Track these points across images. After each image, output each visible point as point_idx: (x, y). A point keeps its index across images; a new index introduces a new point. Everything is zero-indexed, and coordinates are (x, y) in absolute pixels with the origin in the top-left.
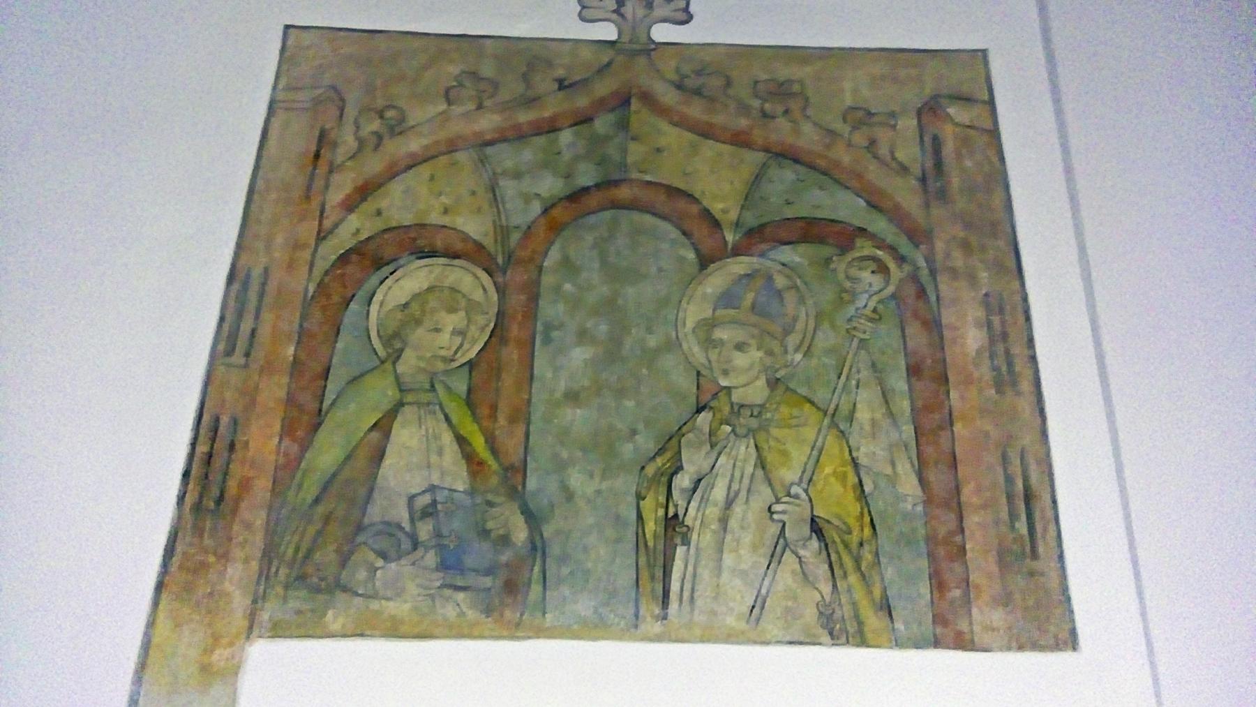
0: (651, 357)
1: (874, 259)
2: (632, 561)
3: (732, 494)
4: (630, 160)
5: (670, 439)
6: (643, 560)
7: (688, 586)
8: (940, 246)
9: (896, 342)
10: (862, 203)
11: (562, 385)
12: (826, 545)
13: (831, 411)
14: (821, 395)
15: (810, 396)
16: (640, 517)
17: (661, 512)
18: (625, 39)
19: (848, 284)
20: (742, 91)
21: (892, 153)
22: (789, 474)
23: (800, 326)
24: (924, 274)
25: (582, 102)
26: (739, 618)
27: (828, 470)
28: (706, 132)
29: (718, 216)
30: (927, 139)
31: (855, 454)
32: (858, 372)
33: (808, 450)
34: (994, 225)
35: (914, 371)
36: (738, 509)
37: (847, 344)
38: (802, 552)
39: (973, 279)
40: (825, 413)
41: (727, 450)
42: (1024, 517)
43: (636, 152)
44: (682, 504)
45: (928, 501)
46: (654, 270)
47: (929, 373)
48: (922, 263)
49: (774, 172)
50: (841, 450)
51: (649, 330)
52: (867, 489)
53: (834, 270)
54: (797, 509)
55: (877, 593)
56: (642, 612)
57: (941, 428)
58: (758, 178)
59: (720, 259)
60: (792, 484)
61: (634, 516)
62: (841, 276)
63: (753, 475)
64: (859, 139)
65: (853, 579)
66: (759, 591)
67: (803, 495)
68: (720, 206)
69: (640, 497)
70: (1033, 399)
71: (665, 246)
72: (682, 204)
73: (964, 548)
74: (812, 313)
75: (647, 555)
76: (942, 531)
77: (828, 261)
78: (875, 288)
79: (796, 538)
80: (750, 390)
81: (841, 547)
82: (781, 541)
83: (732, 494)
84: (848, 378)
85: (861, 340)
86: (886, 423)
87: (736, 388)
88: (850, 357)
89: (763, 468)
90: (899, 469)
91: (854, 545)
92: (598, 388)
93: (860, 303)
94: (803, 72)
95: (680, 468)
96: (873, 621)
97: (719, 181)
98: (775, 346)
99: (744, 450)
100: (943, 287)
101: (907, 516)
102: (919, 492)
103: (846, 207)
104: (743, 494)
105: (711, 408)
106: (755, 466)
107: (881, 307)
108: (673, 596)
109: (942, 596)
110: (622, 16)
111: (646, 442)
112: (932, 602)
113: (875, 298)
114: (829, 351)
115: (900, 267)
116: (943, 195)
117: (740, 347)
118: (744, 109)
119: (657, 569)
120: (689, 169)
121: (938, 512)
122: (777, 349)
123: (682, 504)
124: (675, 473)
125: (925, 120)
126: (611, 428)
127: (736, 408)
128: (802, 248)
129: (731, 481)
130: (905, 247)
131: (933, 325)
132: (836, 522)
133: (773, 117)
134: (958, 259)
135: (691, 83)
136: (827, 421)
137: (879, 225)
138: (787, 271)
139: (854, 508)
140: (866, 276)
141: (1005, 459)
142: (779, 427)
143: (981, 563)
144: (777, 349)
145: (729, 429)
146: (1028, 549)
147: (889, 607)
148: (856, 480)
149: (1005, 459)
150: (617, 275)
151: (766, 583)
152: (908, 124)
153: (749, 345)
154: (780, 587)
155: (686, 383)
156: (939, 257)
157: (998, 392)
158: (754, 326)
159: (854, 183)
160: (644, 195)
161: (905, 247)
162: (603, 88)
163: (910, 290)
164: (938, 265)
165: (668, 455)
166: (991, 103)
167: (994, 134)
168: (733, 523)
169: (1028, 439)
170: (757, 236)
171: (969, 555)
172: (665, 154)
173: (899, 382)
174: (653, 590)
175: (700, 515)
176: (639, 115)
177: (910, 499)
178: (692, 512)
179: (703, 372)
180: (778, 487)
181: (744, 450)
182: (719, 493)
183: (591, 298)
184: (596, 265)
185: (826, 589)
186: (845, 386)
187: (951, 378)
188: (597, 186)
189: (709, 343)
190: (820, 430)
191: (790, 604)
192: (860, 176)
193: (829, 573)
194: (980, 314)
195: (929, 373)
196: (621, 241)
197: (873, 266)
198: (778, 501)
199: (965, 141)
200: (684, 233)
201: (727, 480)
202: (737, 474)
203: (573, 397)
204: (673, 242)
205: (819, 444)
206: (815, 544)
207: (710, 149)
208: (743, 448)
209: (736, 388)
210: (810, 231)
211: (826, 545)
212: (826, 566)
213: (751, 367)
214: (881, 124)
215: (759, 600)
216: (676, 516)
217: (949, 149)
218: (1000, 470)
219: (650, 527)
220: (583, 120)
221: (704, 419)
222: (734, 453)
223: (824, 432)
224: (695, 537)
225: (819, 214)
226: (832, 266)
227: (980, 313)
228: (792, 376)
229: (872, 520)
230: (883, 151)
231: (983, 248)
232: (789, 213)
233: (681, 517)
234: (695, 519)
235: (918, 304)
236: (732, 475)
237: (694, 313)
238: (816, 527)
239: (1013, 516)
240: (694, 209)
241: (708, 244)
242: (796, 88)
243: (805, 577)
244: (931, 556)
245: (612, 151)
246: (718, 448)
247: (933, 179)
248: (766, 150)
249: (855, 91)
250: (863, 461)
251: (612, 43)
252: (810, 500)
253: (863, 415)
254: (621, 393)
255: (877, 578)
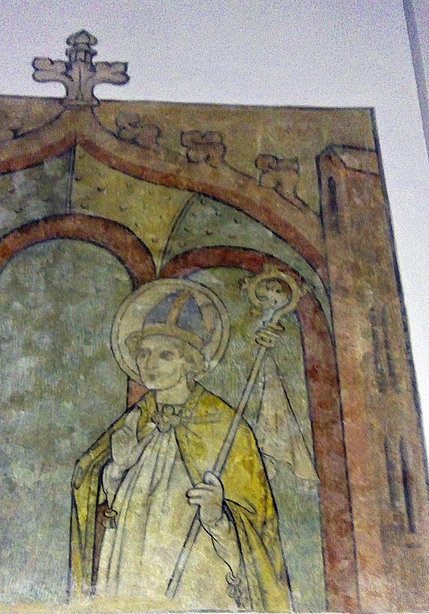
0: (87, 365)
1: (280, 281)
2: (65, 543)
3: (155, 482)
4: (74, 198)
5: (103, 435)
6: (75, 541)
7: (114, 564)
8: (333, 269)
9: (297, 351)
10: (270, 234)
11: (9, 391)
12: (235, 525)
13: (241, 409)
14: (233, 396)
15: (223, 396)
16: (74, 505)
17: (93, 500)
18: (72, 97)
19: (257, 302)
20: (171, 140)
21: (295, 192)
22: (204, 463)
23: (216, 336)
24: (321, 293)
25: (34, 148)
26: (158, 591)
27: (238, 459)
28: (140, 175)
29: (149, 244)
30: (324, 182)
31: (260, 445)
32: (264, 375)
33: (221, 443)
34: (378, 250)
35: (311, 374)
36: (159, 495)
37: (255, 352)
38: (214, 531)
39: (360, 297)
40: (236, 412)
41: (152, 444)
42: (402, 498)
43: (79, 190)
44: (111, 492)
45: (322, 484)
46: (92, 291)
47: (325, 375)
48: (318, 283)
49: (197, 208)
50: (249, 442)
51: (87, 342)
52: (270, 476)
53: (246, 290)
54: (211, 493)
55: (278, 564)
56: (73, 588)
57: (334, 422)
58: (182, 214)
59: (149, 281)
60: (206, 473)
61: (68, 503)
62: (252, 295)
63: (174, 464)
64: (269, 180)
65: (258, 553)
66: (177, 566)
67: (217, 482)
68: (151, 236)
69: (74, 486)
70: (410, 395)
71: (103, 270)
72: (119, 235)
73: (352, 524)
74: (227, 327)
75: (80, 538)
76: (333, 509)
77: (241, 282)
78: (280, 305)
79: (209, 518)
80: (172, 392)
81: (247, 525)
82: (197, 522)
83: (155, 482)
84: (255, 382)
85: (268, 349)
86: (287, 419)
87: (160, 390)
88: (258, 363)
89: (183, 460)
90: (298, 456)
91: (258, 525)
92: (41, 392)
93: (267, 318)
94: (218, 125)
95: (111, 460)
96: (275, 590)
97: (149, 215)
98: (195, 353)
99: (166, 445)
100: (336, 305)
101: (305, 499)
102: (314, 477)
103: (255, 237)
104: (164, 482)
105: (139, 408)
106: (176, 458)
107: (284, 320)
108: (101, 574)
109: (333, 567)
110: (70, 77)
111: (81, 439)
112: (325, 572)
113: (279, 314)
114: (243, 358)
115: (300, 287)
116: (336, 226)
117: (164, 355)
118: (173, 157)
119: (87, 550)
120: (124, 206)
121: (329, 493)
122: (196, 357)
123: (111, 492)
124: (106, 464)
125: (322, 164)
126: (51, 427)
127: (160, 408)
128: (219, 272)
129: (155, 471)
130: (305, 271)
131: (327, 336)
132: (244, 504)
133: (197, 163)
134: (349, 281)
135: (127, 134)
136: (238, 417)
137: (284, 253)
138: (207, 291)
139: (259, 491)
140: (272, 295)
141: (386, 449)
142: (195, 423)
143: (367, 538)
144: (196, 357)
145: (153, 425)
146: (406, 525)
147: (288, 577)
148: (262, 467)
149: (386, 449)
150: (61, 296)
151: (183, 559)
152: (308, 169)
153: (173, 354)
154: (194, 562)
155: (118, 387)
156: (333, 277)
157: (381, 391)
158: (177, 337)
159: (263, 217)
160: (86, 228)
161: (305, 271)
162: (52, 137)
163: (310, 306)
164: (332, 286)
165: (101, 449)
166: (377, 151)
167: (379, 176)
168: (156, 508)
169: (404, 429)
170: (183, 261)
171: (356, 529)
172: (105, 192)
173: (298, 384)
174: (83, 568)
175: (126, 502)
176: (84, 161)
177: (306, 483)
178: (119, 498)
179: (133, 377)
180: (194, 474)
181: (166, 445)
182: (144, 482)
183: (37, 315)
184: (42, 287)
185: (234, 562)
186: (253, 387)
187: (342, 379)
188: (46, 219)
189: (139, 352)
190: (231, 425)
191: (203, 577)
192: (267, 211)
193: (238, 552)
194: (366, 326)
195: (325, 375)
196: (65, 266)
197: (279, 286)
198: (194, 487)
199: (354, 183)
200: (120, 259)
201: (152, 469)
202: (160, 464)
203: (17, 400)
204: (110, 267)
205: (230, 437)
206: (225, 524)
207: (142, 189)
208: (165, 441)
209: (160, 390)
210: (228, 258)
211: (235, 525)
212: (235, 543)
213: (175, 370)
214: (288, 168)
215: (177, 576)
216: (106, 502)
217: (342, 189)
218: (382, 456)
219: (83, 512)
220: (33, 164)
221: (132, 418)
222: (157, 447)
223: (235, 426)
224: (121, 521)
225: (233, 243)
226: (244, 286)
227: (367, 325)
228: (207, 380)
229: (274, 501)
230: (288, 191)
231: (370, 273)
232: (209, 242)
233: (110, 505)
234: (123, 504)
235: (315, 319)
236: (156, 465)
237: (127, 325)
238: (226, 509)
239: (393, 496)
240: (129, 239)
241: (142, 268)
242: (216, 139)
243: (217, 554)
244: (325, 533)
245: (59, 190)
246: (145, 441)
247: (329, 213)
248: (190, 190)
249: (265, 140)
250: (267, 450)
251: (61, 101)
252: (222, 486)
253: (268, 412)
254: (60, 397)
255: (279, 556)
